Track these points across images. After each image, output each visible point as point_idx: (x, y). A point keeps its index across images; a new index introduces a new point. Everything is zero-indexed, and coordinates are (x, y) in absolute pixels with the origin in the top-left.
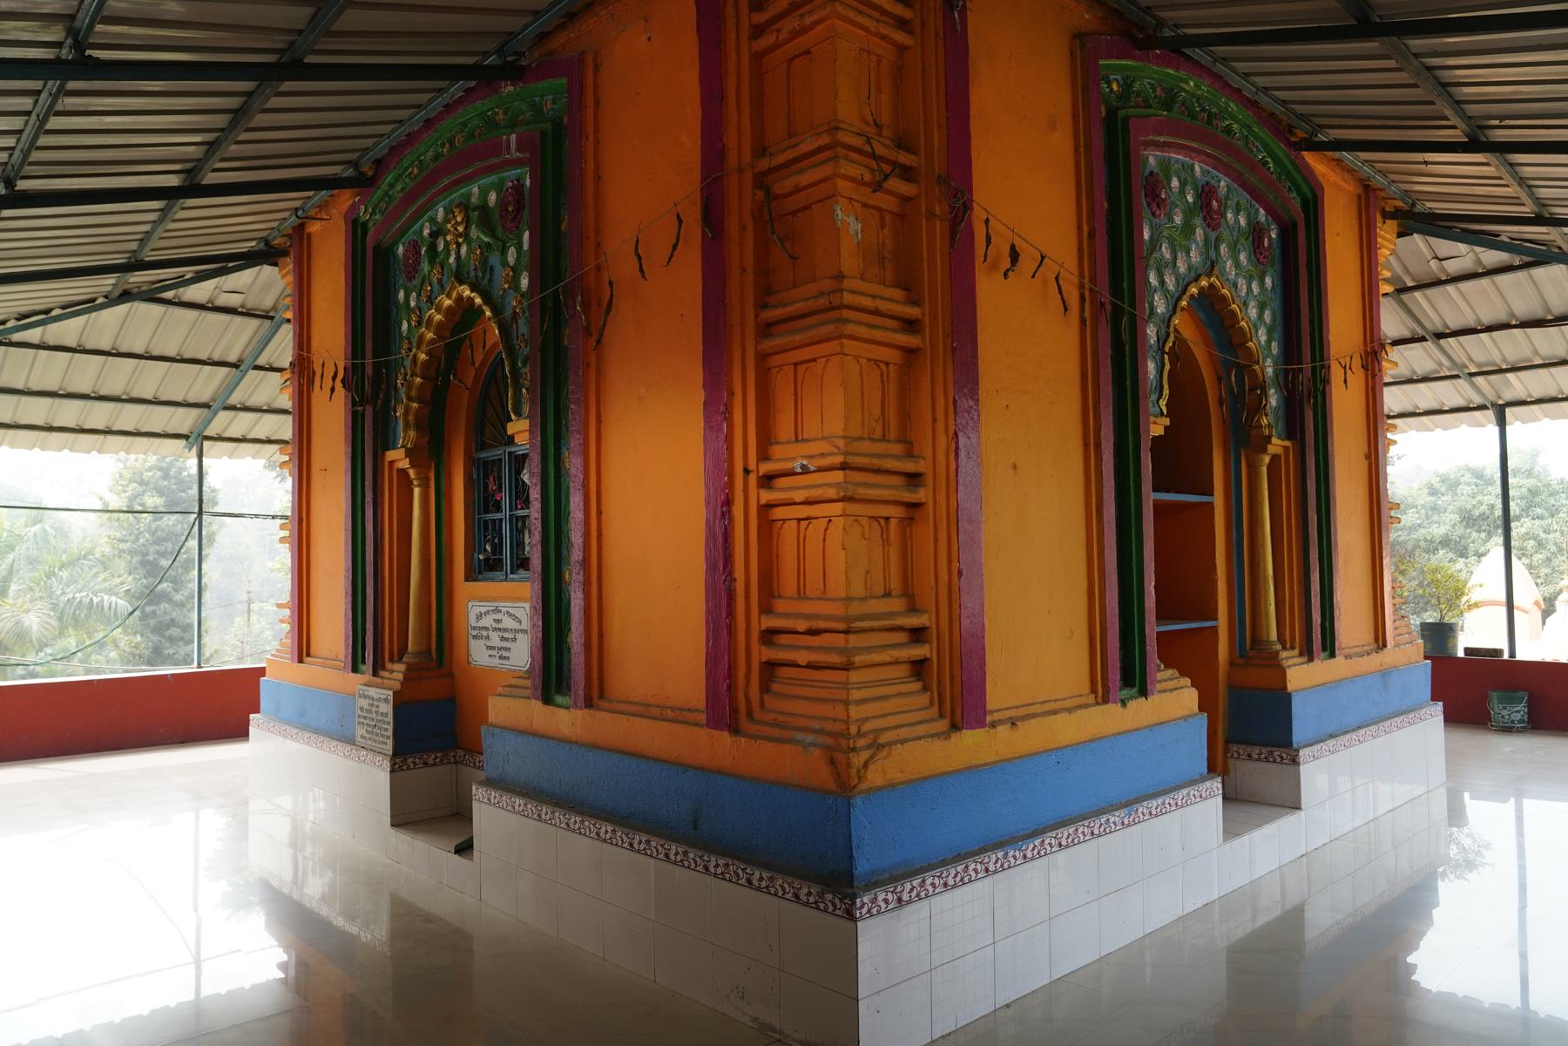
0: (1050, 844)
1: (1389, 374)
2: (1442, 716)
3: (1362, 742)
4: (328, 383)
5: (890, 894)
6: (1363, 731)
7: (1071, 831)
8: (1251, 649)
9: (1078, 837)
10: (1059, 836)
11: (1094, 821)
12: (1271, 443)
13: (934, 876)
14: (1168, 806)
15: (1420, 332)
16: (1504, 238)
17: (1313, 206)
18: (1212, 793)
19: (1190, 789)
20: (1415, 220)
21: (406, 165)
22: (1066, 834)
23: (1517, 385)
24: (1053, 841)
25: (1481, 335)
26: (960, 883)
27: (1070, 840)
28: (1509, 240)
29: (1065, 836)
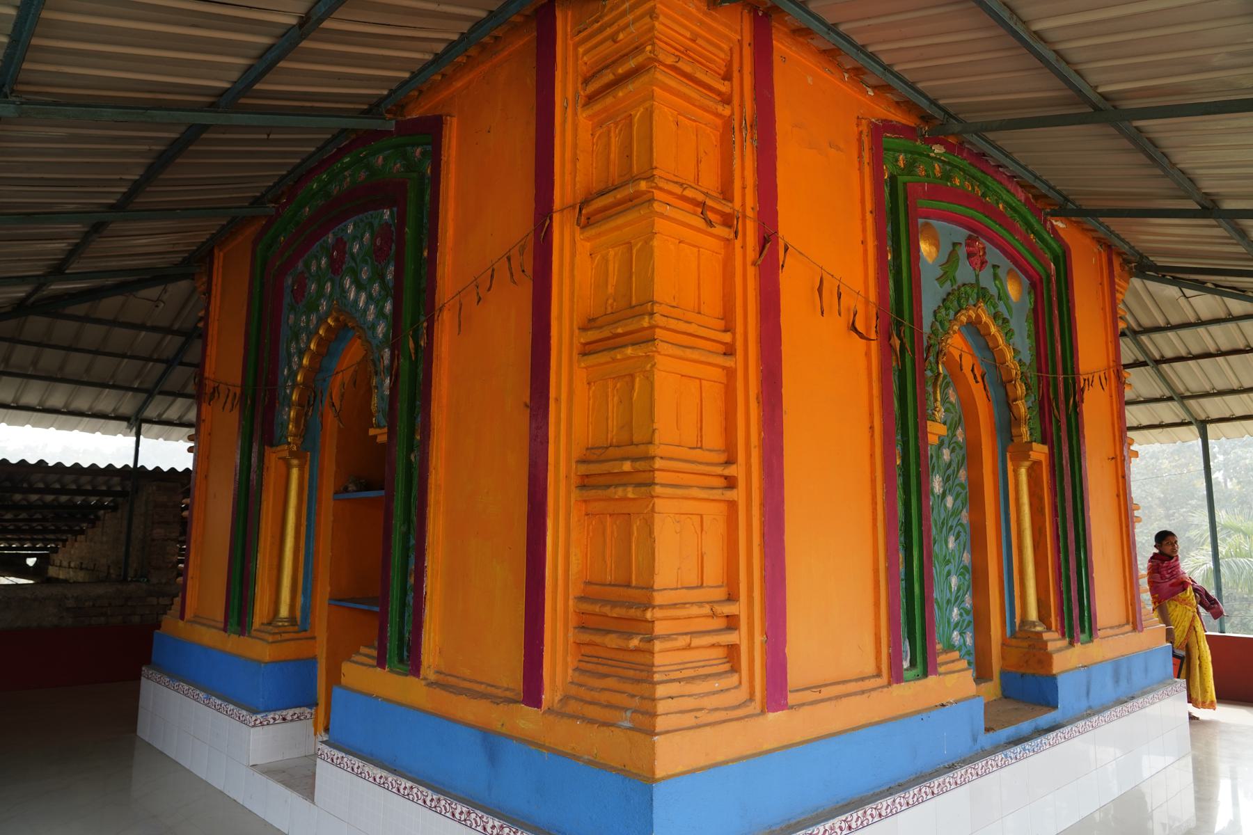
0: (872, 815)
1: (1129, 394)
3: (1095, 728)
4: (222, 399)
5: (874, 810)
6: (1054, 734)
7: (890, 802)
9: (922, 796)
10: (849, 819)
11: (957, 772)
12: (1032, 450)
13: (872, 808)
14: (948, 785)
15: (1141, 358)
16: (1209, 285)
17: (1063, 260)
18: (920, 800)
19: (945, 776)
20: (1144, 267)
21: (1127, 247)
23: (1213, 407)
24: (874, 812)
25: (1217, 358)
27: (859, 823)
28: (1213, 287)
29: (884, 807)
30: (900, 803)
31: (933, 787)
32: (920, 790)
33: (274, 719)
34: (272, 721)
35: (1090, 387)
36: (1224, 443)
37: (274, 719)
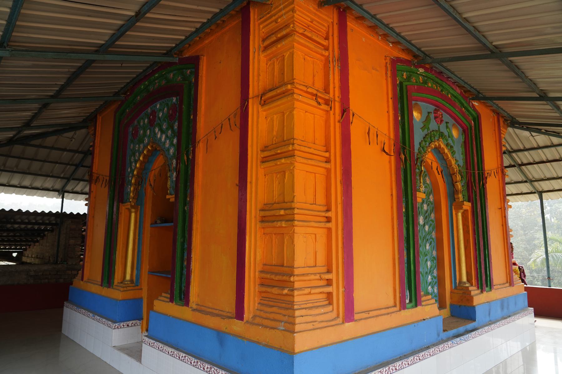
2: (534, 314)
7: (400, 363)
8: (459, 286)
12: (464, 205)
13: (392, 366)
17: (477, 119)
18: (444, 349)
19: (425, 352)
20: (514, 123)
22: (398, 365)
23: (545, 185)
26: (401, 369)
28: (545, 131)
29: (384, 371)
30: (405, 364)
31: (420, 356)
32: (414, 358)
33: (123, 325)
34: (122, 326)
35: (490, 176)
36: (550, 201)
37: (123, 325)
